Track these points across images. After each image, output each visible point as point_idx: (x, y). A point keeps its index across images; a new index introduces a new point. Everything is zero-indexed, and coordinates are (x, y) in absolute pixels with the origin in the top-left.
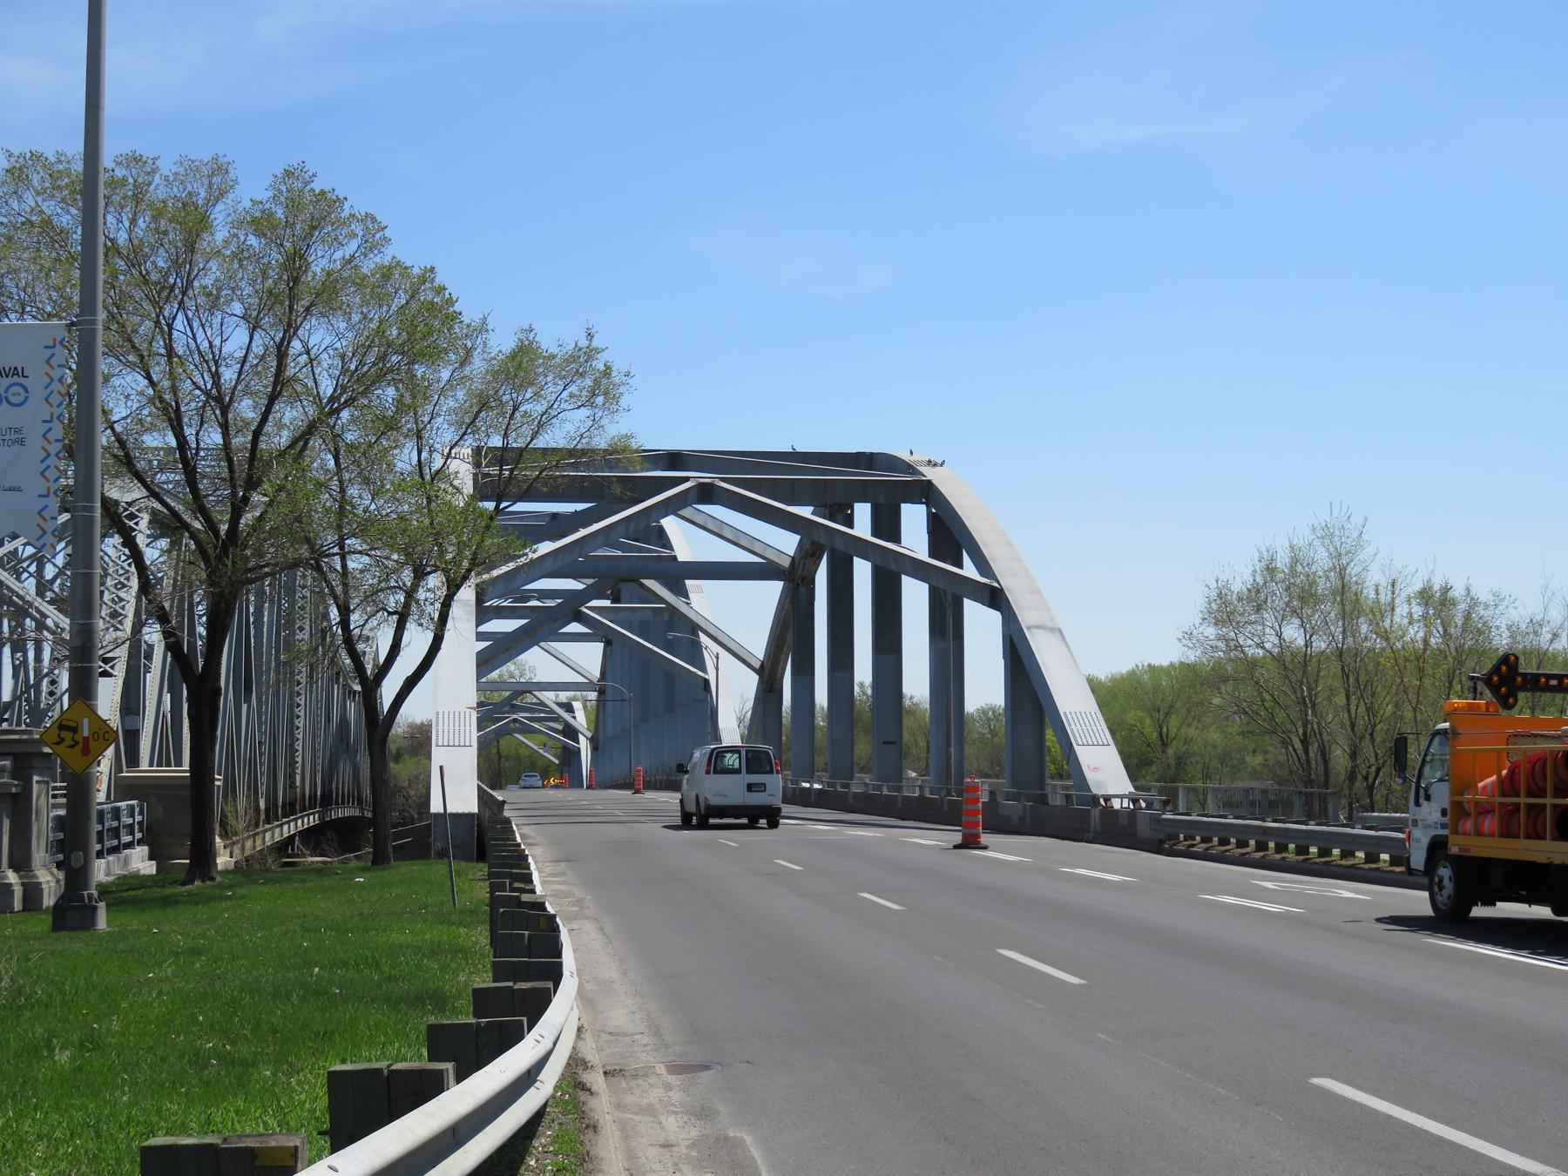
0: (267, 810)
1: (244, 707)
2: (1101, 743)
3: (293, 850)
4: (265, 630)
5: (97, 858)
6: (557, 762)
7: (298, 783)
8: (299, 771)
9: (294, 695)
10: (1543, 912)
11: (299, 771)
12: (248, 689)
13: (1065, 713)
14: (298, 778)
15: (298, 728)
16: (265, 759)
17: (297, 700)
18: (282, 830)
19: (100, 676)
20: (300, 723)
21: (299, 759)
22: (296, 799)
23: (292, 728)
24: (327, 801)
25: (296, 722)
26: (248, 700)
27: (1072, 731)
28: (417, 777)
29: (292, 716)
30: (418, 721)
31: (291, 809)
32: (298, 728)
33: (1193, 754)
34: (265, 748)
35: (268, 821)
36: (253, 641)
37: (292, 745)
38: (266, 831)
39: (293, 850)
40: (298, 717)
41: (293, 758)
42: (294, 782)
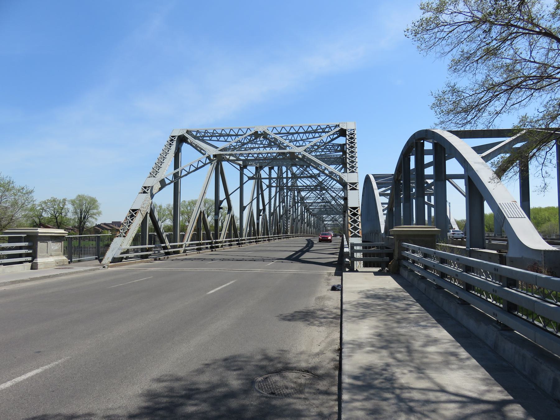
2: (515, 217)
13: (500, 204)
27: (505, 211)
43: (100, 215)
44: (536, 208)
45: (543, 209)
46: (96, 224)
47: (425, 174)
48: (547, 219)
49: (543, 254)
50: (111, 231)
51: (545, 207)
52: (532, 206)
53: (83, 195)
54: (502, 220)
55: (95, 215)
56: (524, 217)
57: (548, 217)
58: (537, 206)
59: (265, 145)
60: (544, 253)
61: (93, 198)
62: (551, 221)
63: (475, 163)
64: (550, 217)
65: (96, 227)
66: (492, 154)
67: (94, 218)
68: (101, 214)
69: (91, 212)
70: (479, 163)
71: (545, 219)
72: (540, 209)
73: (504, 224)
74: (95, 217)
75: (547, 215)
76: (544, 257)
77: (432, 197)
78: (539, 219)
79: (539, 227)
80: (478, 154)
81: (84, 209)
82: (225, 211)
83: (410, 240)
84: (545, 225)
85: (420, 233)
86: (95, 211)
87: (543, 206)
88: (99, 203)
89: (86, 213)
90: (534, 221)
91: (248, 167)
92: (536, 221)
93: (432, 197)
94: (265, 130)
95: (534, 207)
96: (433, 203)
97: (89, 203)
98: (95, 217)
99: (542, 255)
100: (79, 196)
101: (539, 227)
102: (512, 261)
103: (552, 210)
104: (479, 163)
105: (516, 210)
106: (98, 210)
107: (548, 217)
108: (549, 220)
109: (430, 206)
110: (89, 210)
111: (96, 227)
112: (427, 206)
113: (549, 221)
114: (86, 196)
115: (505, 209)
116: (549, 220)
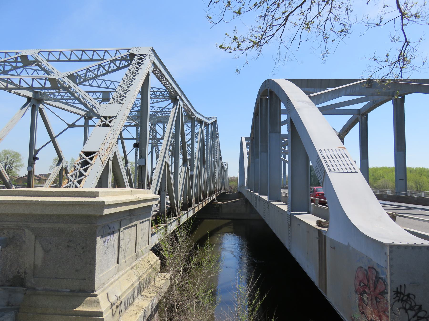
0: (209, 193)
1: (203, 169)
2: (345, 171)
3: (215, 201)
4: (209, 153)
5: (168, 218)
6: (4, 185)
7: (216, 187)
8: (216, 184)
9: (215, 168)
10: (66, 91)
11: (216, 184)
12: (204, 164)
13: (320, 150)
14: (216, 186)
15: (216, 175)
16: (209, 181)
17: (216, 169)
18: (212, 197)
19: (180, 159)
20: (216, 174)
21: (216, 182)
22: (215, 190)
23: (215, 175)
24: (221, 189)
25: (215, 174)
26: (204, 166)
27: (326, 162)
28: (233, 185)
29: (215, 173)
30: (232, 177)
31: (214, 192)
32: (216, 175)
33: (425, 172)
34: (209, 179)
35: (209, 196)
36: (206, 155)
37: (215, 179)
38: (209, 198)
39: (215, 201)
40: (216, 173)
41: (215, 181)
42: (215, 187)
43: (23, 167)
44: (374, 168)
45: (379, 168)
46: (25, 175)
47: (281, 134)
48: (382, 176)
49: (388, 254)
50: (38, 181)
51: (380, 167)
52: (370, 166)
53: (8, 150)
54: (321, 174)
55: (19, 167)
56: (354, 171)
57: (383, 175)
58: (374, 166)
59: (138, 106)
60: (391, 252)
61: (17, 152)
62: (384, 178)
63: (298, 101)
64: (384, 174)
65: (24, 177)
66: (323, 96)
67: (17, 169)
68: (23, 166)
69: (15, 164)
70: (303, 102)
71: (381, 176)
72: (376, 169)
73: (324, 182)
74: (18, 168)
75: (382, 173)
76: (391, 259)
77: (287, 156)
78: (376, 176)
79: (376, 182)
80: (323, 114)
81: (8, 162)
82: (133, 166)
83: (26, 231)
84: (380, 181)
85: (48, 211)
86: (18, 163)
87: (379, 166)
88: (22, 157)
89: (10, 165)
90: (373, 177)
91: (93, 119)
92: (373, 177)
93: (287, 156)
94: (34, 54)
95: (372, 167)
96: (287, 159)
97: (13, 157)
98: (18, 168)
99: (386, 254)
100: (5, 151)
101: (376, 182)
102: (334, 248)
103: (385, 169)
104: (303, 102)
105: (344, 161)
106: (21, 163)
107: (383, 175)
108: (383, 177)
109: (285, 162)
110: (13, 162)
111: (24, 177)
112: (287, 164)
113: (383, 178)
114: (10, 151)
115: (327, 159)
116: (383, 177)
